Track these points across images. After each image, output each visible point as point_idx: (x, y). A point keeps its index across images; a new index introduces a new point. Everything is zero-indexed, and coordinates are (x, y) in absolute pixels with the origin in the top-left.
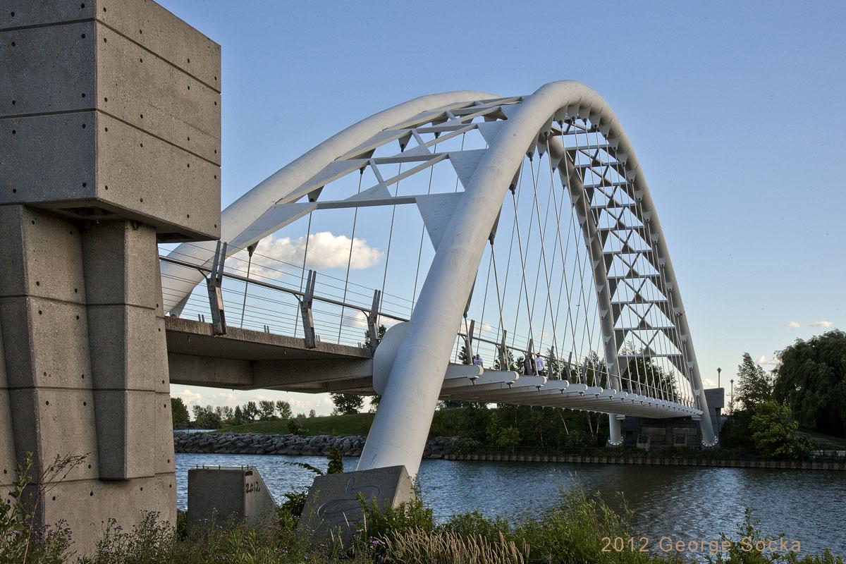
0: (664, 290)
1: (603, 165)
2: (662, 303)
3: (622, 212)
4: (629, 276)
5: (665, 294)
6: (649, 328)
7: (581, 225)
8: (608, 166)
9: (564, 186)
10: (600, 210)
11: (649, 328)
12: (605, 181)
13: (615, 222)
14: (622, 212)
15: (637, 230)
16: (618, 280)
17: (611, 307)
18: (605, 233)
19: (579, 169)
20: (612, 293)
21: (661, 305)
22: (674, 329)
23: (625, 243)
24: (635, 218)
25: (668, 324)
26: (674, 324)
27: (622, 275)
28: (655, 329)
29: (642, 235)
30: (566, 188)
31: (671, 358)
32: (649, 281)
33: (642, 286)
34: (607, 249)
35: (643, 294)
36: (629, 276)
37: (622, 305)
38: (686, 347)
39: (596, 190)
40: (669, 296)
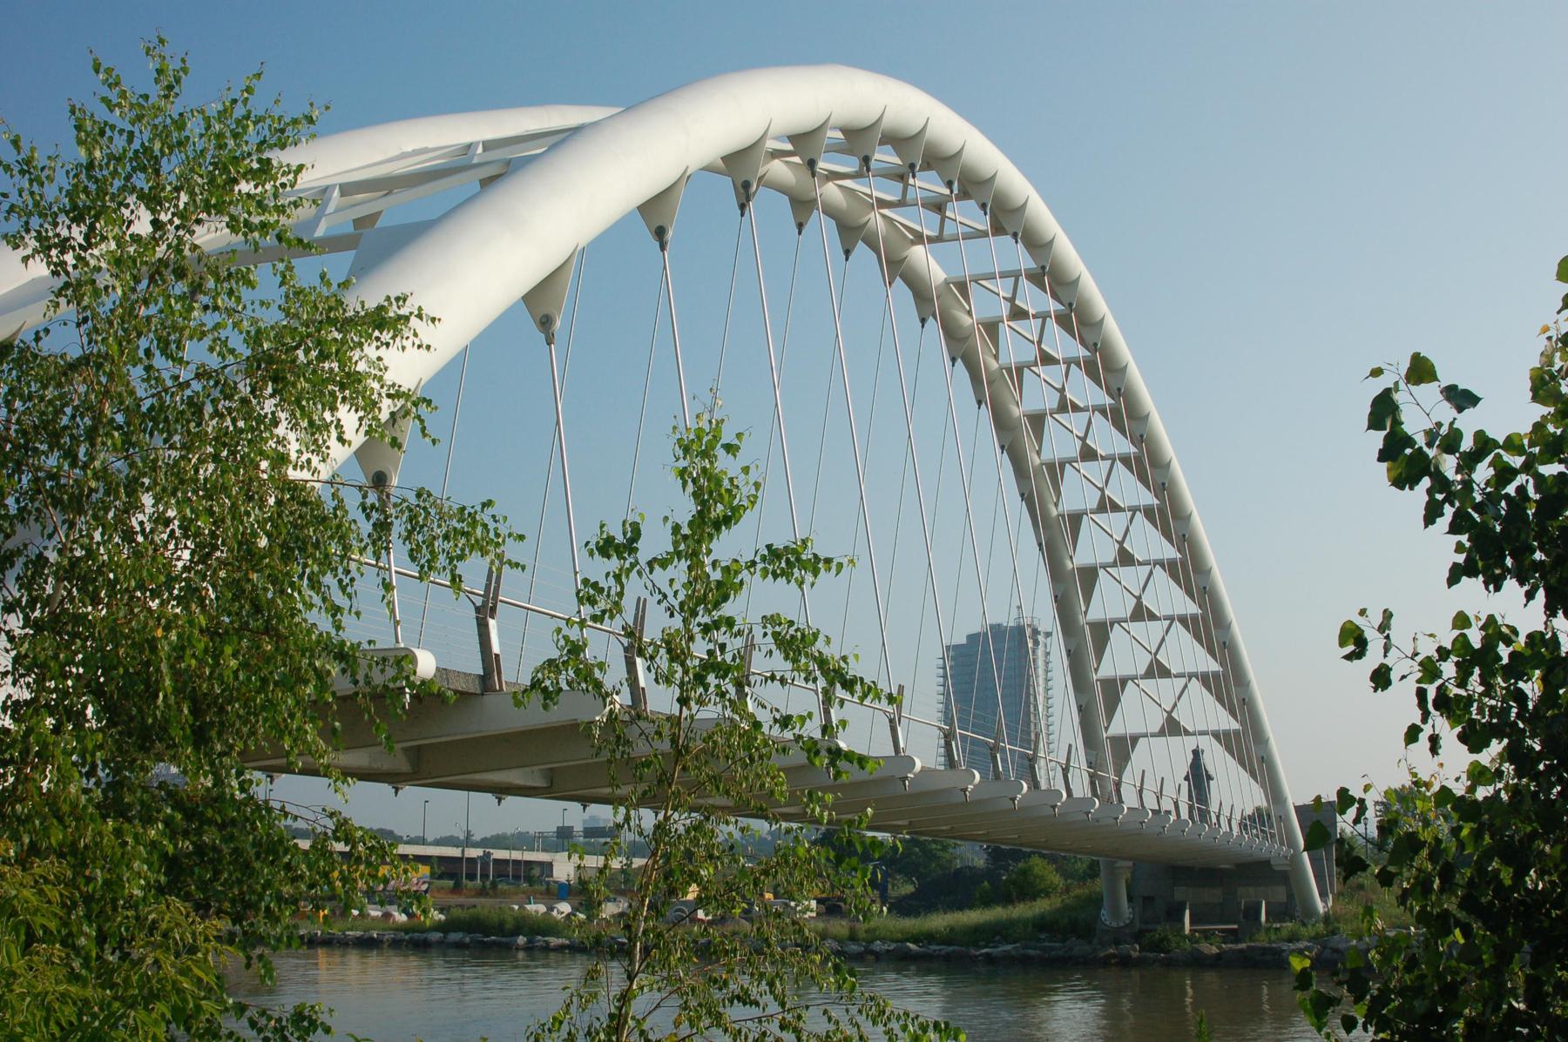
0: (1251, 764)
1: (1103, 458)
2: (1227, 733)
3: (1186, 686)
4: (1149, 674)
5: (1233, 714)
6: (1153, 617)
7: (1002, 447)
8: (1114, 460)
9: (979, 403)
10: (1062, 465)
11: (1153, 617)
12: (1159, 663)
13: (1131, 603)
14: (1186, 686)
15: (1163, 566)
16: (1112, 625)
17: (1098, 688)
18: (1075, 519)
19: (1009, 370)
20: (1110, 714)
21: (1171, 568)
22: (1184, 563)
23: (1139, 598)
24: (1154, 535)
25: (1170, 552)
26: (1235, 717)
27: (1130, 672)
28: (1146, 563)
29: (1174, 576)
30: (983, 406)
31: (1221, 737)
32: (1195, 684)
33: (1179, 698)
34: (1107, 668)
35: (1183, 718)
36: (1149, 674)
37: (1124, 681)
38: (1163, 487)
39: (1101, 572)
40: (1243, 714)
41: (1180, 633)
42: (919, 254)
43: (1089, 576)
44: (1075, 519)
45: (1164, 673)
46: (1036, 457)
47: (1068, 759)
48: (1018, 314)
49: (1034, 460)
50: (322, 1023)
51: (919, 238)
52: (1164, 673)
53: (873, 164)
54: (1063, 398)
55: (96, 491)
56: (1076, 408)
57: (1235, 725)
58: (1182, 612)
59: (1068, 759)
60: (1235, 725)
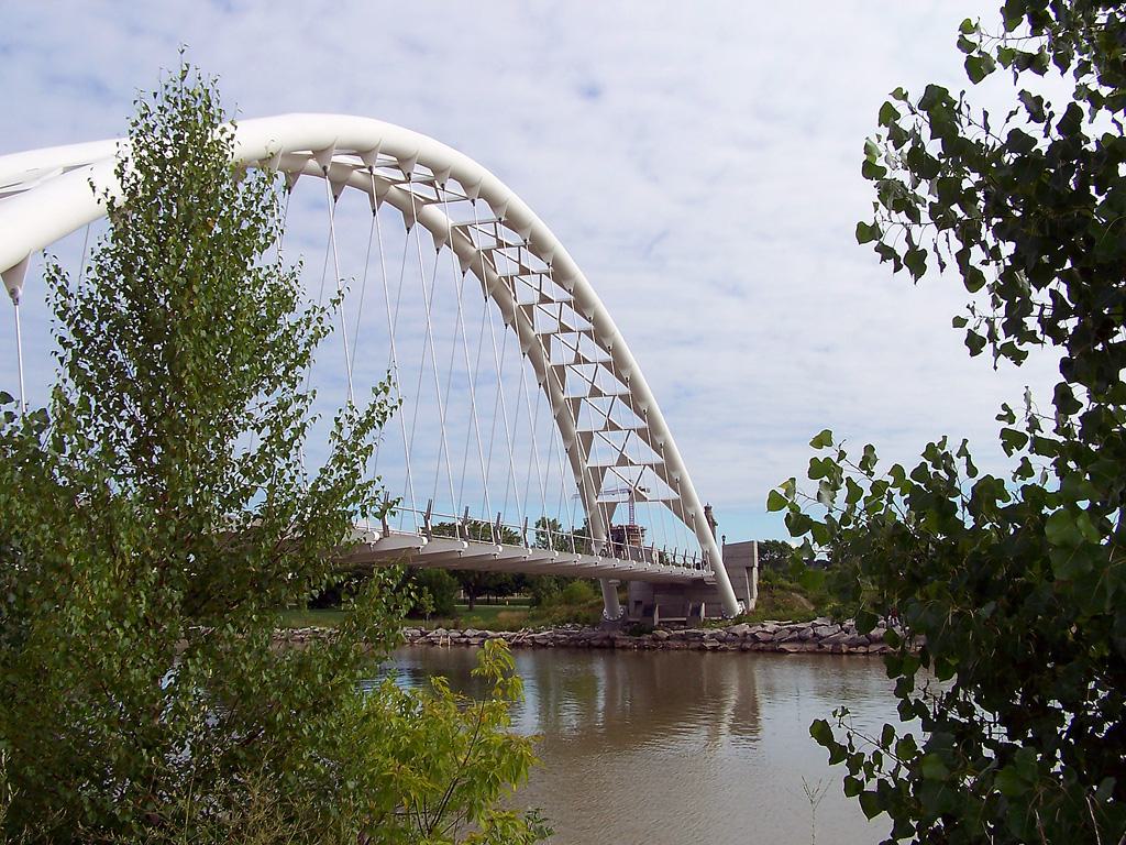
15: (651, 466)
18: (576, 402)
21: (641, 433)
36: (605, 429)
39: (595, 435)
41: (635, 438)
42: (432, 210)
43: (588, 437)
44: (576, 402)
45: (614, 427)
46: (514, 302)
47: (429, 510)
48: (545, 300)
49: (547, 365)
50: (849, 479)
51: (430, 201)
52: (614, 427)
53: (413, 176)
54: (578, 355)
55: (890, 628)
56: (586, 361)
57: (677, 496)
58: (640, 427)
59: (429, 510)
60: (677, 496)
